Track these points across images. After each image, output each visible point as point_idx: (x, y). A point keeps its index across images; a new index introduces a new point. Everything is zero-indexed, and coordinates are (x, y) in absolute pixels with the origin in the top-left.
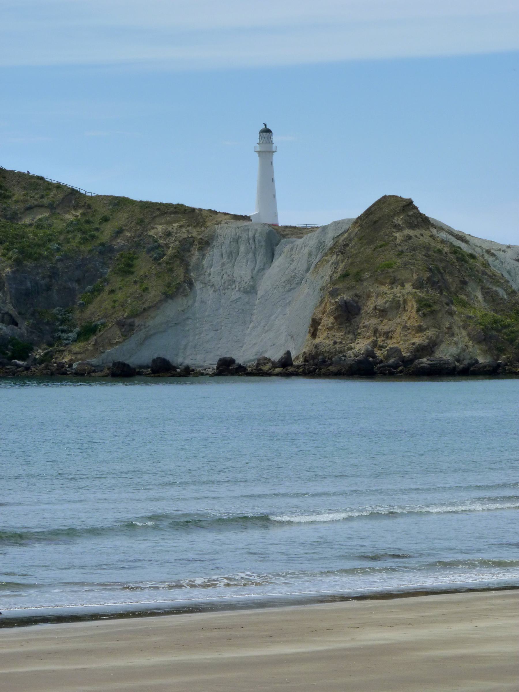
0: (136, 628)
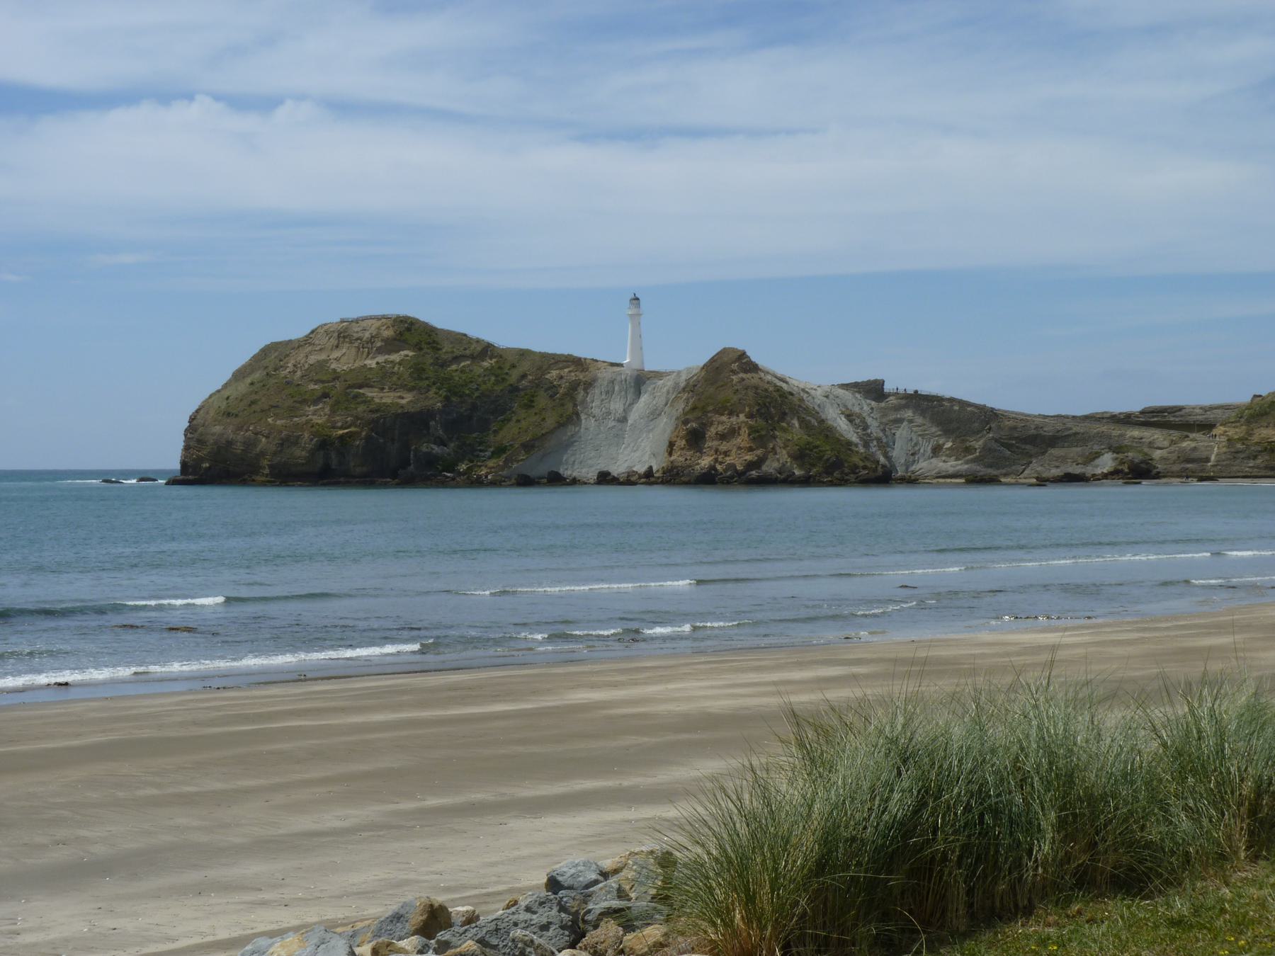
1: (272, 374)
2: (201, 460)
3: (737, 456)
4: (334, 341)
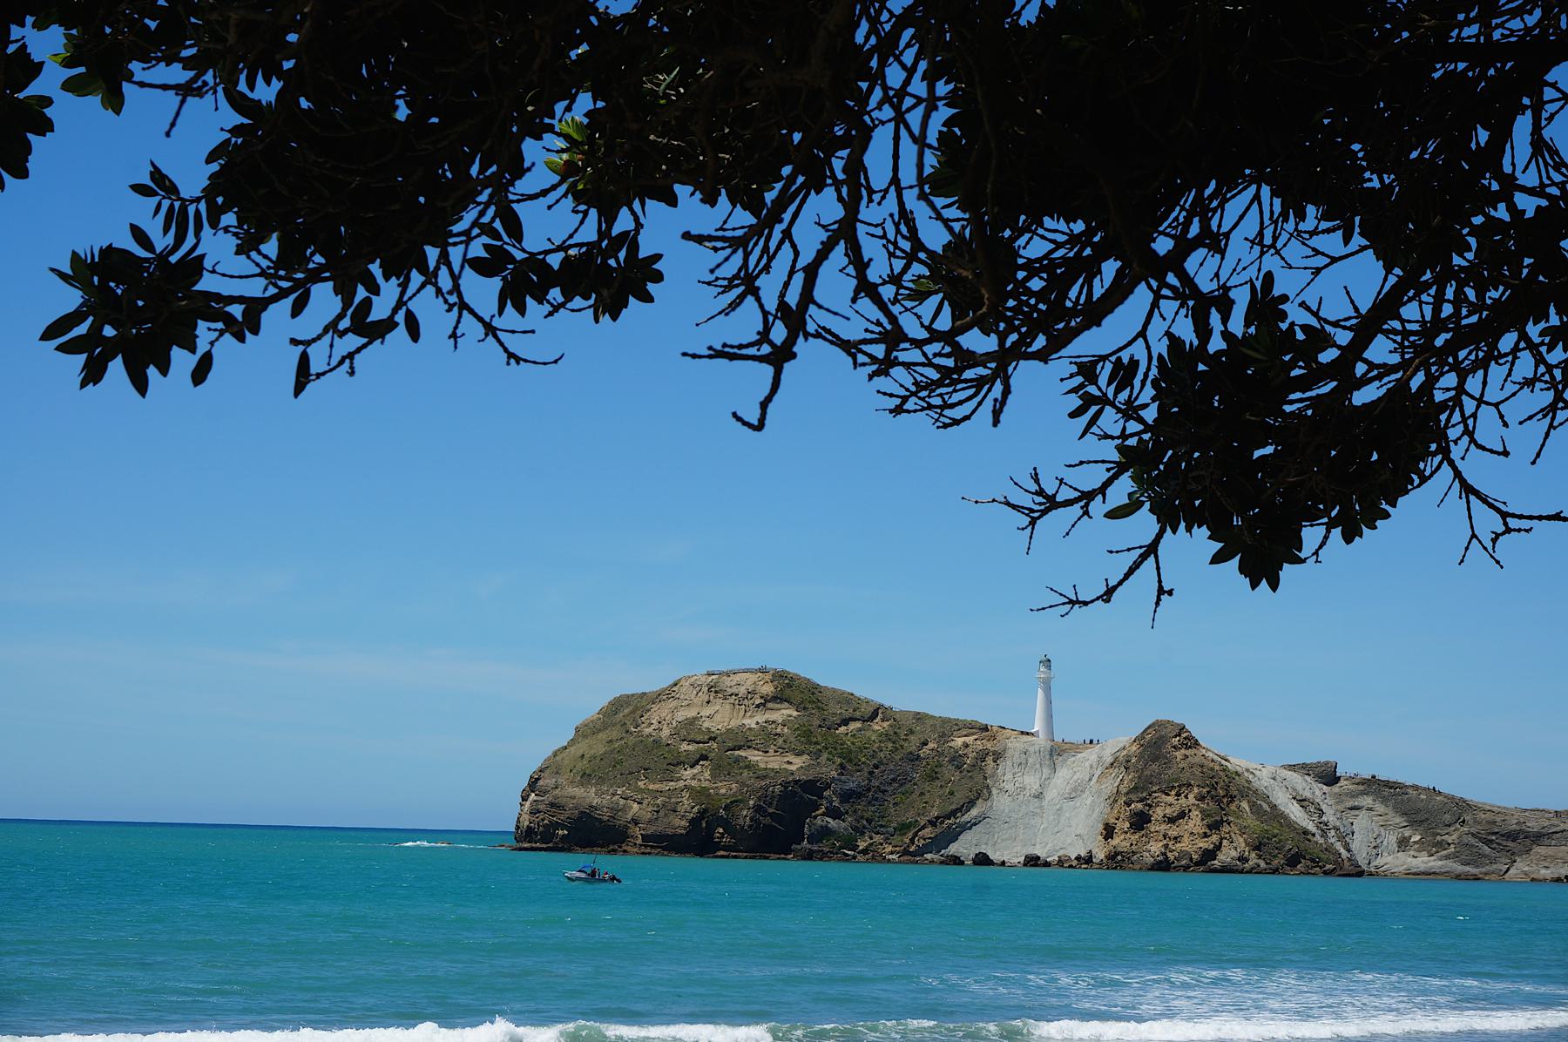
0: (1542, 989)
1: (623, 736)
2: (557, 826)
3: (1191, 837)
4: (704, 697)
